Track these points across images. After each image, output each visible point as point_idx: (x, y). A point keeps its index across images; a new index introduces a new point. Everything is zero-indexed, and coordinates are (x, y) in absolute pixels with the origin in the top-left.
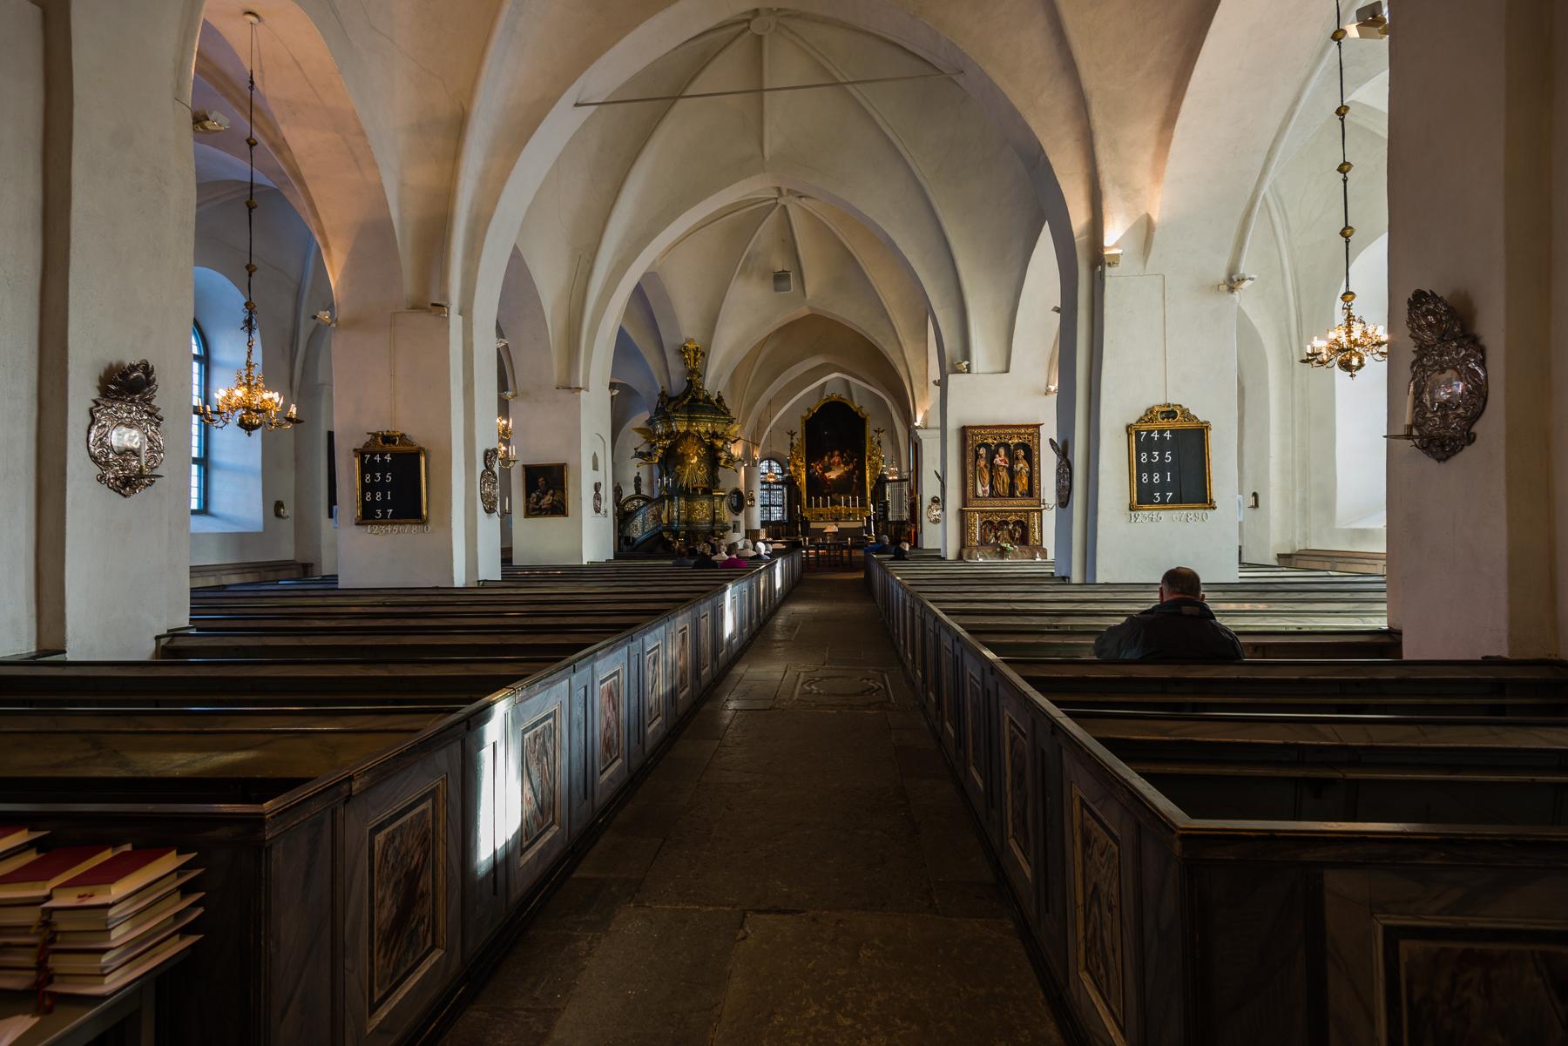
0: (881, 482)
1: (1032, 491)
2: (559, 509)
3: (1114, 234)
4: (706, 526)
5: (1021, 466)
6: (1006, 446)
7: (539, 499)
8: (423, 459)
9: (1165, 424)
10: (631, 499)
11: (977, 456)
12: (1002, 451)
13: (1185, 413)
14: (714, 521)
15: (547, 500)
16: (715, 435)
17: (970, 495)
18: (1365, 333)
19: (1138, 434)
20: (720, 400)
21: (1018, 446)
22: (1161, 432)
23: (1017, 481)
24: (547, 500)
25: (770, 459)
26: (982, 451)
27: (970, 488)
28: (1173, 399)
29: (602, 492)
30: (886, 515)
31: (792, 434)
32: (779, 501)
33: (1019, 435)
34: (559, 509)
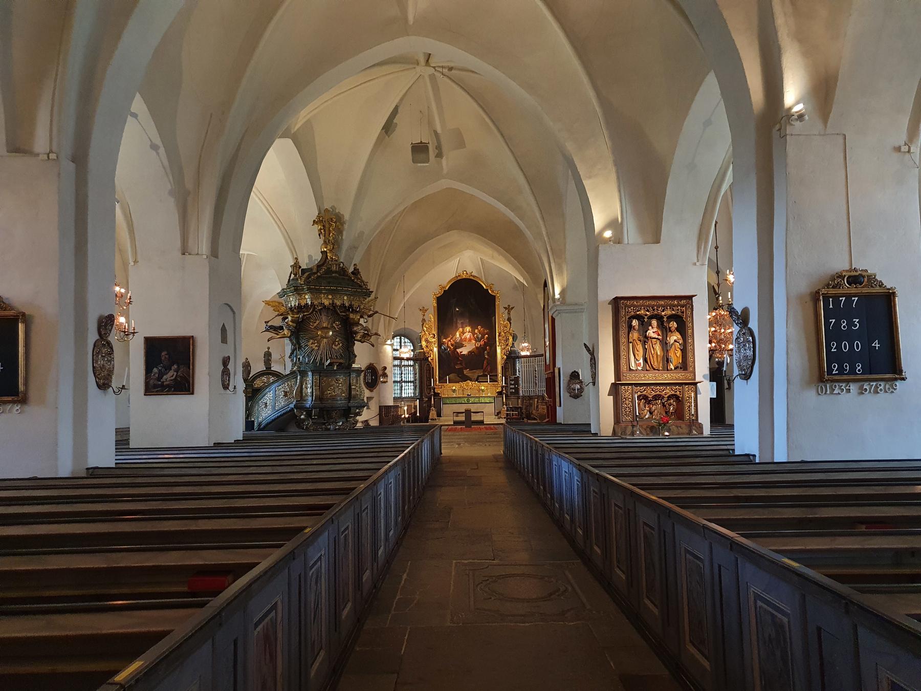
0: (512, 357)
1: (686, 364)
2: (184, 386)
3: (793, 94)
4: (341, 402)
5: (674, 337)
6: (659, 318)
7: (161, 375)
8: (21, 327)
9: (853, 290)
10: (261, 374)
11: (630, 327)
12: (654, 322)
13: (872, 279)
14: (350, 397)
15: (170, 376)
16: (350, 309)
17: (624, 367)
18: (392, 345)
19: (826, 298)
20: (356, 272)
21: (671, 318)
22: (849, 297)
23: (671, 354)
24: (170, 376)
25: (400, 336)
26: (635, 323)
27: (623, 361)
28: (861, 264)
29: (230, 366)
30: (517, 390)
31: (424, 310)
32: (411, 377)
33: (672, 307)
34: (184, 386)
